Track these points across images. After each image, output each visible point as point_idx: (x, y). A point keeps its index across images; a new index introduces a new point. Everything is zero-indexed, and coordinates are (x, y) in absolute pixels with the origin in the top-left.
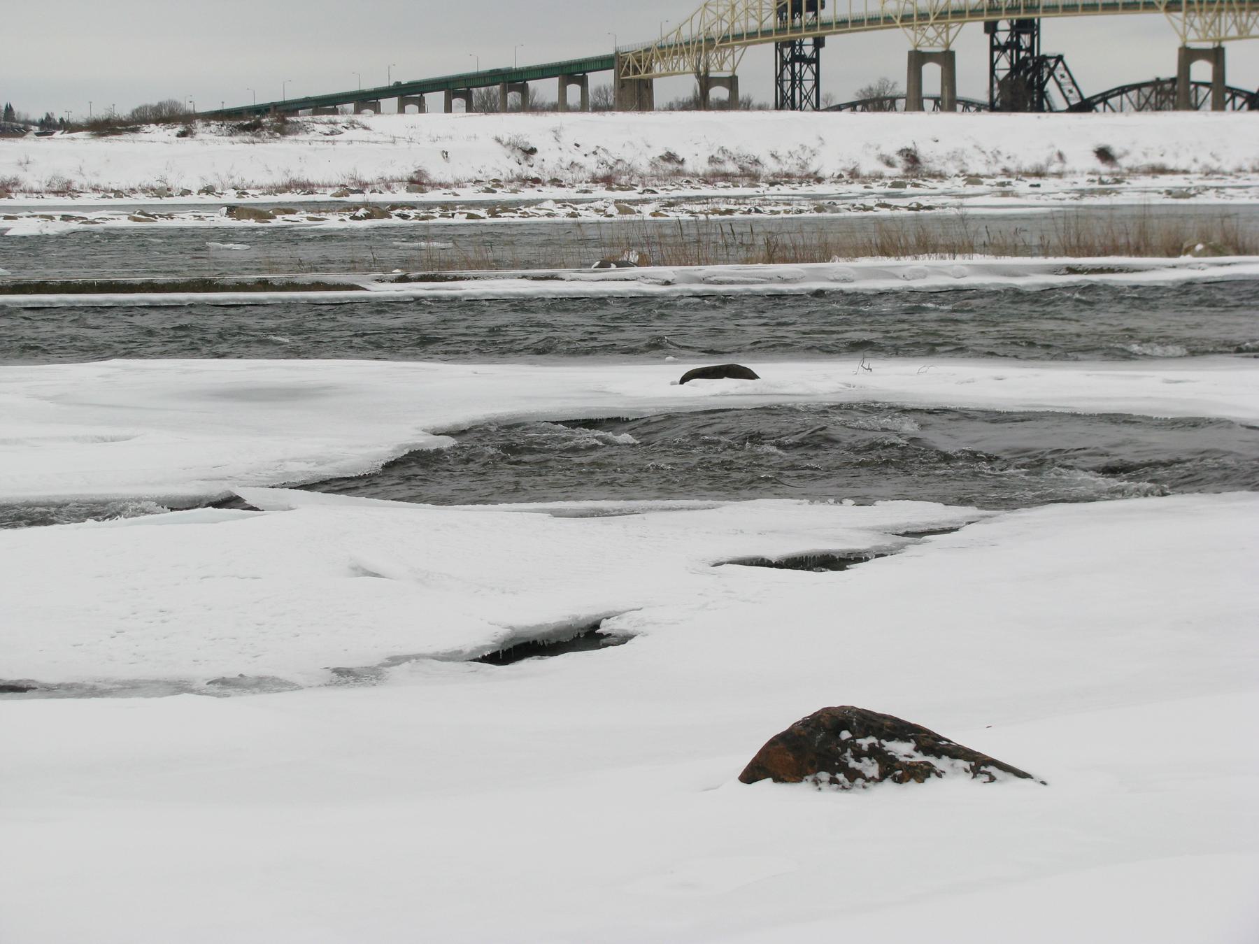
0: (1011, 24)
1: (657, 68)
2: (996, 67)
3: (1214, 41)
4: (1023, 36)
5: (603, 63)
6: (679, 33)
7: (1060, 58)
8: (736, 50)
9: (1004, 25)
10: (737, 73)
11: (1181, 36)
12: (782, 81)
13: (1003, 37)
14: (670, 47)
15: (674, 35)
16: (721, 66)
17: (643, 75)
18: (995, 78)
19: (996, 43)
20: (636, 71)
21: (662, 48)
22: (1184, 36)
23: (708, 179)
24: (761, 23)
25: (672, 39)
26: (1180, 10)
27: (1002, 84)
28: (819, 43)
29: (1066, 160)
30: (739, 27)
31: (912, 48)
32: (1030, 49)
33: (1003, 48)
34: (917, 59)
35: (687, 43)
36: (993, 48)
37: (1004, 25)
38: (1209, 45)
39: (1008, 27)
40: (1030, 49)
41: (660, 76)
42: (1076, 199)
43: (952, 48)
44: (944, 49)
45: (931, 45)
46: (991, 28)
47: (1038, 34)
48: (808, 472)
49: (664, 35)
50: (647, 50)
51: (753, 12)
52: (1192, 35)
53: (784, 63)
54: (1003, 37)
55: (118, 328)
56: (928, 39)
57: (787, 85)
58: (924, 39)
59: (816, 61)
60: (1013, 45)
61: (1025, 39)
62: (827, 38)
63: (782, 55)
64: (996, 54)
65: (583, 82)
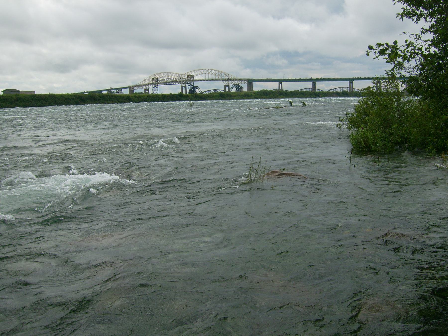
7: (198, 87)
32: (193, 85)
38: (227, 85)
53: (153, 87)
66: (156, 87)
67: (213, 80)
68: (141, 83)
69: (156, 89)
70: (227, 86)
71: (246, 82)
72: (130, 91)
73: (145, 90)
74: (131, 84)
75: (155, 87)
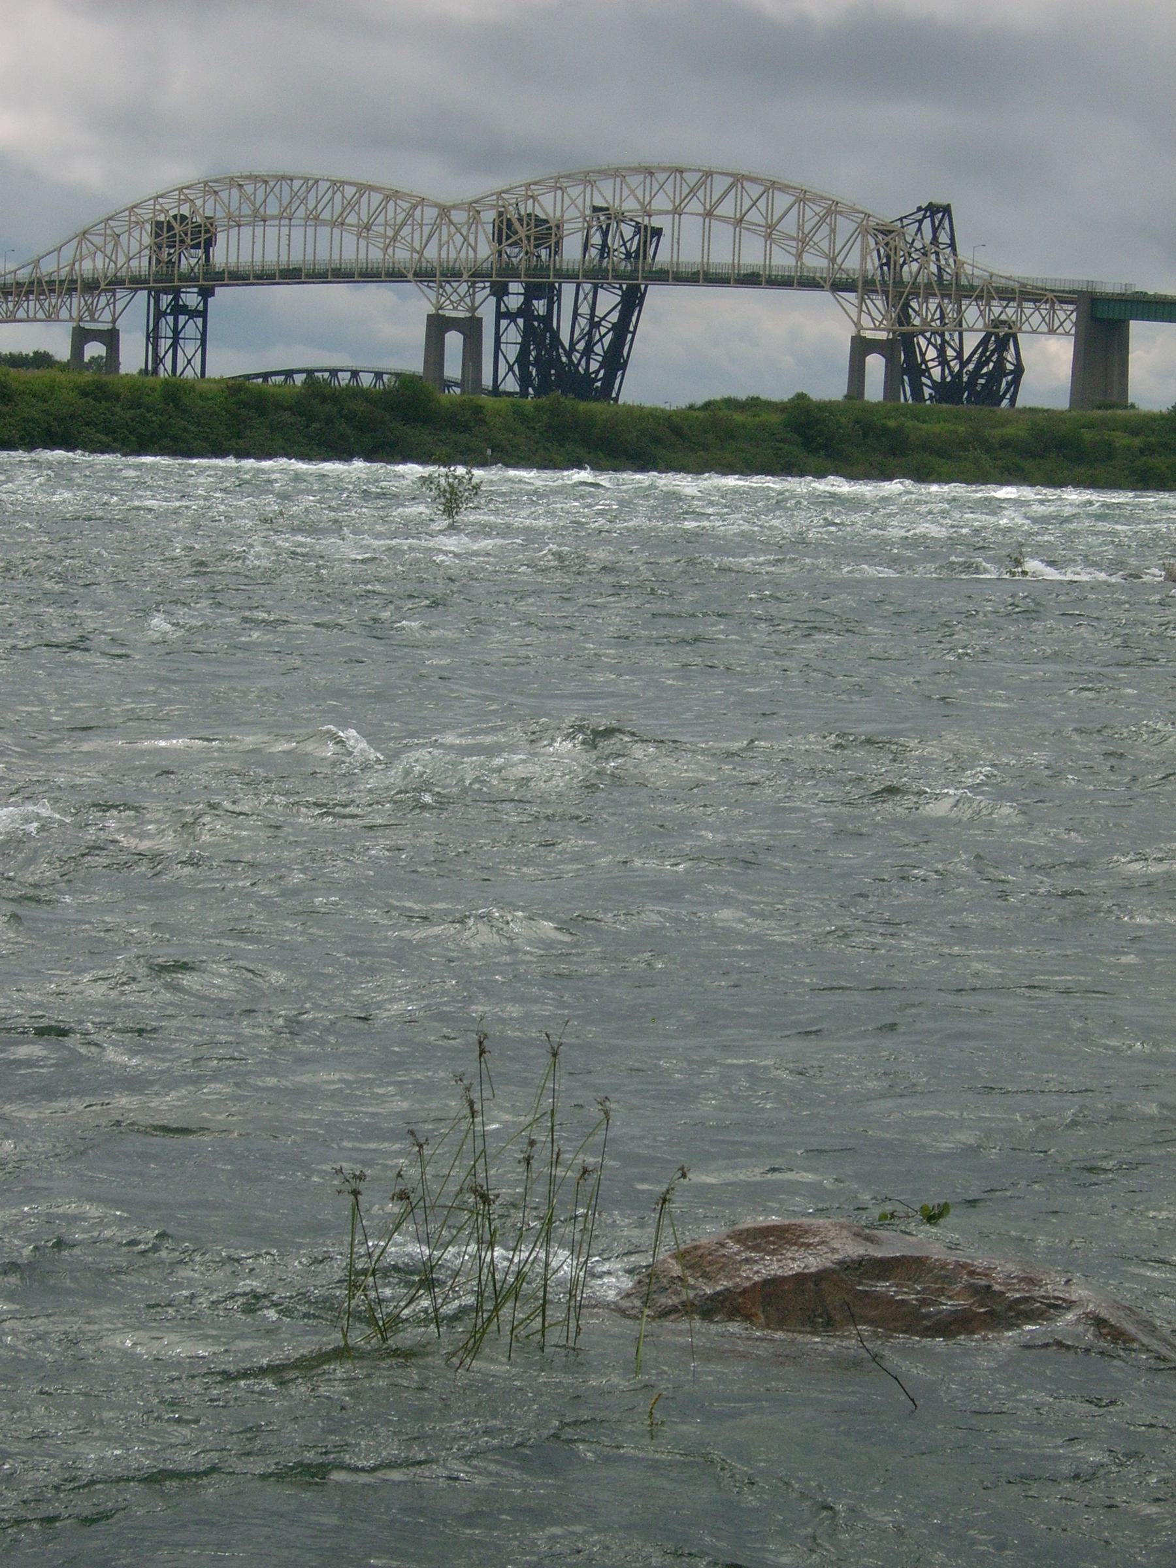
2: (503, 339)
4: (535, 302)
6: (72, 269)
8: (118, 296)
9: (515, 287)
10: (118, 325)
11: (855, 324)
12: (157, 338)
13: (514, 302)
18: (501, 356)
19: (503, 309)
22: (858, 325)
28: (206, 293)
30: (87, 267)
31: (432, 311)
33: (511, 316)
34: (438, 326)
37: (515, 287)
43: (478, 314)
44: (468, 315)
45: (455, 309)
46: (500, 291)
47: (559, 300)
48: (593, 1202)
49: (479, 261)
52: (866, 321)
53: (159, 315)
56: (452, 302)
57: (164, 344)
58: (448, 302)
59: (203, 314)
60: (525, 311)
61: (540, 306)
62: (217, 289)
63: (157, 303)
64: (201, 308)
66: (193, 314)
67: (751, 279)
68: (48, 267)
69: (191, 329)
71: (1067, 316)
73: (81, 337)
75: (179, 309)
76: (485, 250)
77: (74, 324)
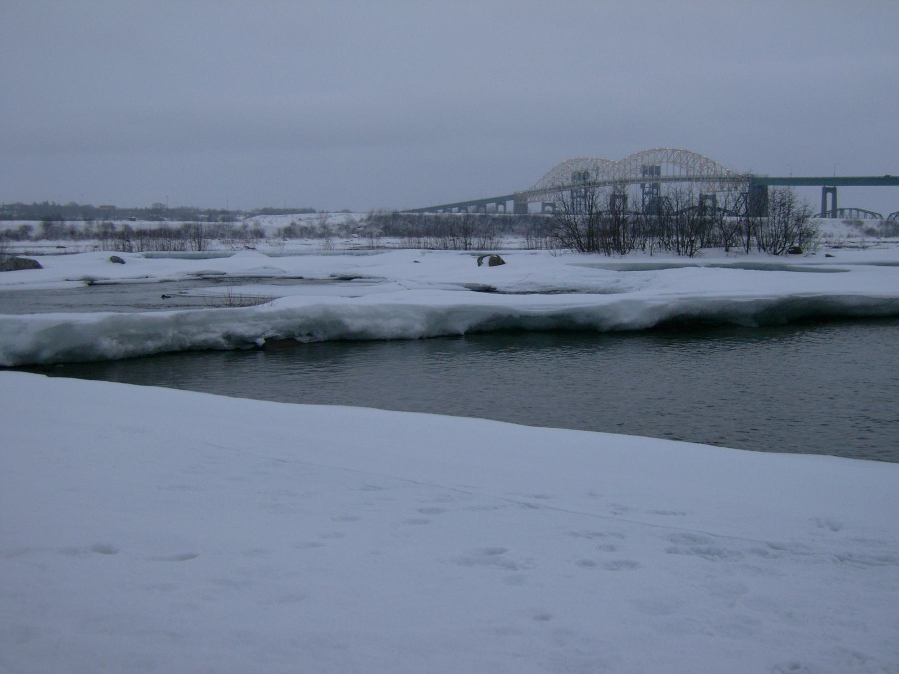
0: (650, 185)
1: (529, 200)
3: (712, 192)
5: (510, 198)
9: (647, 185)
14: (532, 192)
15: (533, 188)
16: (550, 198)
17: (523, 202)
20: (521, 201)
21: (529, 192)
23: (478, 249)
24: (637, 175)
25: (533, 189)
26: (700, 181)
27: (646, 207)
29: (42, 266)
32: (657, 194)
33: (647, 194)
35: (538, 191)
36: (643, 194)
39: (649, 186)
40: (657, 194)
41: (530, 202)
42: (876, 246)
46: (643, 186)
50: (525, 193)
51: (633, 172)
52: (704, 190)
54: (647, 190)
55: (133, 297)
65: (505, 205)
68: (537, 187)
70: (618, 197)
72: (517, 206)
74: (521, 188)
76: (640, 176)
77: (542, 202)
